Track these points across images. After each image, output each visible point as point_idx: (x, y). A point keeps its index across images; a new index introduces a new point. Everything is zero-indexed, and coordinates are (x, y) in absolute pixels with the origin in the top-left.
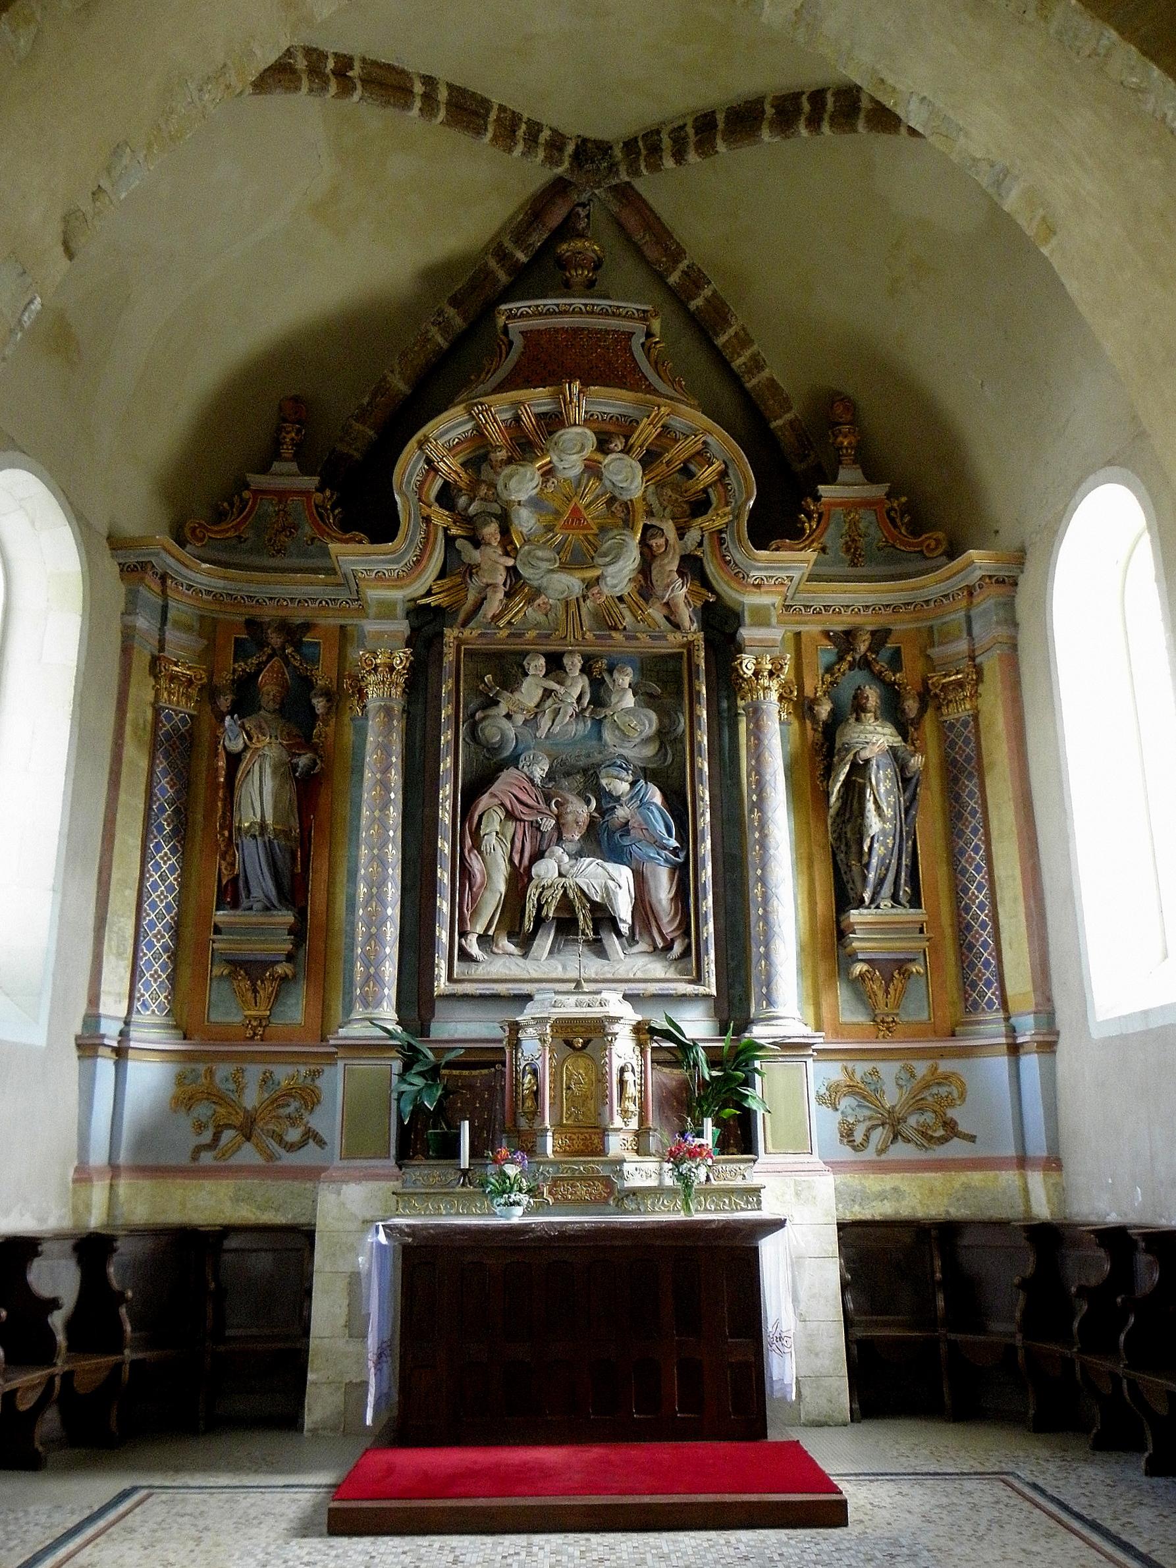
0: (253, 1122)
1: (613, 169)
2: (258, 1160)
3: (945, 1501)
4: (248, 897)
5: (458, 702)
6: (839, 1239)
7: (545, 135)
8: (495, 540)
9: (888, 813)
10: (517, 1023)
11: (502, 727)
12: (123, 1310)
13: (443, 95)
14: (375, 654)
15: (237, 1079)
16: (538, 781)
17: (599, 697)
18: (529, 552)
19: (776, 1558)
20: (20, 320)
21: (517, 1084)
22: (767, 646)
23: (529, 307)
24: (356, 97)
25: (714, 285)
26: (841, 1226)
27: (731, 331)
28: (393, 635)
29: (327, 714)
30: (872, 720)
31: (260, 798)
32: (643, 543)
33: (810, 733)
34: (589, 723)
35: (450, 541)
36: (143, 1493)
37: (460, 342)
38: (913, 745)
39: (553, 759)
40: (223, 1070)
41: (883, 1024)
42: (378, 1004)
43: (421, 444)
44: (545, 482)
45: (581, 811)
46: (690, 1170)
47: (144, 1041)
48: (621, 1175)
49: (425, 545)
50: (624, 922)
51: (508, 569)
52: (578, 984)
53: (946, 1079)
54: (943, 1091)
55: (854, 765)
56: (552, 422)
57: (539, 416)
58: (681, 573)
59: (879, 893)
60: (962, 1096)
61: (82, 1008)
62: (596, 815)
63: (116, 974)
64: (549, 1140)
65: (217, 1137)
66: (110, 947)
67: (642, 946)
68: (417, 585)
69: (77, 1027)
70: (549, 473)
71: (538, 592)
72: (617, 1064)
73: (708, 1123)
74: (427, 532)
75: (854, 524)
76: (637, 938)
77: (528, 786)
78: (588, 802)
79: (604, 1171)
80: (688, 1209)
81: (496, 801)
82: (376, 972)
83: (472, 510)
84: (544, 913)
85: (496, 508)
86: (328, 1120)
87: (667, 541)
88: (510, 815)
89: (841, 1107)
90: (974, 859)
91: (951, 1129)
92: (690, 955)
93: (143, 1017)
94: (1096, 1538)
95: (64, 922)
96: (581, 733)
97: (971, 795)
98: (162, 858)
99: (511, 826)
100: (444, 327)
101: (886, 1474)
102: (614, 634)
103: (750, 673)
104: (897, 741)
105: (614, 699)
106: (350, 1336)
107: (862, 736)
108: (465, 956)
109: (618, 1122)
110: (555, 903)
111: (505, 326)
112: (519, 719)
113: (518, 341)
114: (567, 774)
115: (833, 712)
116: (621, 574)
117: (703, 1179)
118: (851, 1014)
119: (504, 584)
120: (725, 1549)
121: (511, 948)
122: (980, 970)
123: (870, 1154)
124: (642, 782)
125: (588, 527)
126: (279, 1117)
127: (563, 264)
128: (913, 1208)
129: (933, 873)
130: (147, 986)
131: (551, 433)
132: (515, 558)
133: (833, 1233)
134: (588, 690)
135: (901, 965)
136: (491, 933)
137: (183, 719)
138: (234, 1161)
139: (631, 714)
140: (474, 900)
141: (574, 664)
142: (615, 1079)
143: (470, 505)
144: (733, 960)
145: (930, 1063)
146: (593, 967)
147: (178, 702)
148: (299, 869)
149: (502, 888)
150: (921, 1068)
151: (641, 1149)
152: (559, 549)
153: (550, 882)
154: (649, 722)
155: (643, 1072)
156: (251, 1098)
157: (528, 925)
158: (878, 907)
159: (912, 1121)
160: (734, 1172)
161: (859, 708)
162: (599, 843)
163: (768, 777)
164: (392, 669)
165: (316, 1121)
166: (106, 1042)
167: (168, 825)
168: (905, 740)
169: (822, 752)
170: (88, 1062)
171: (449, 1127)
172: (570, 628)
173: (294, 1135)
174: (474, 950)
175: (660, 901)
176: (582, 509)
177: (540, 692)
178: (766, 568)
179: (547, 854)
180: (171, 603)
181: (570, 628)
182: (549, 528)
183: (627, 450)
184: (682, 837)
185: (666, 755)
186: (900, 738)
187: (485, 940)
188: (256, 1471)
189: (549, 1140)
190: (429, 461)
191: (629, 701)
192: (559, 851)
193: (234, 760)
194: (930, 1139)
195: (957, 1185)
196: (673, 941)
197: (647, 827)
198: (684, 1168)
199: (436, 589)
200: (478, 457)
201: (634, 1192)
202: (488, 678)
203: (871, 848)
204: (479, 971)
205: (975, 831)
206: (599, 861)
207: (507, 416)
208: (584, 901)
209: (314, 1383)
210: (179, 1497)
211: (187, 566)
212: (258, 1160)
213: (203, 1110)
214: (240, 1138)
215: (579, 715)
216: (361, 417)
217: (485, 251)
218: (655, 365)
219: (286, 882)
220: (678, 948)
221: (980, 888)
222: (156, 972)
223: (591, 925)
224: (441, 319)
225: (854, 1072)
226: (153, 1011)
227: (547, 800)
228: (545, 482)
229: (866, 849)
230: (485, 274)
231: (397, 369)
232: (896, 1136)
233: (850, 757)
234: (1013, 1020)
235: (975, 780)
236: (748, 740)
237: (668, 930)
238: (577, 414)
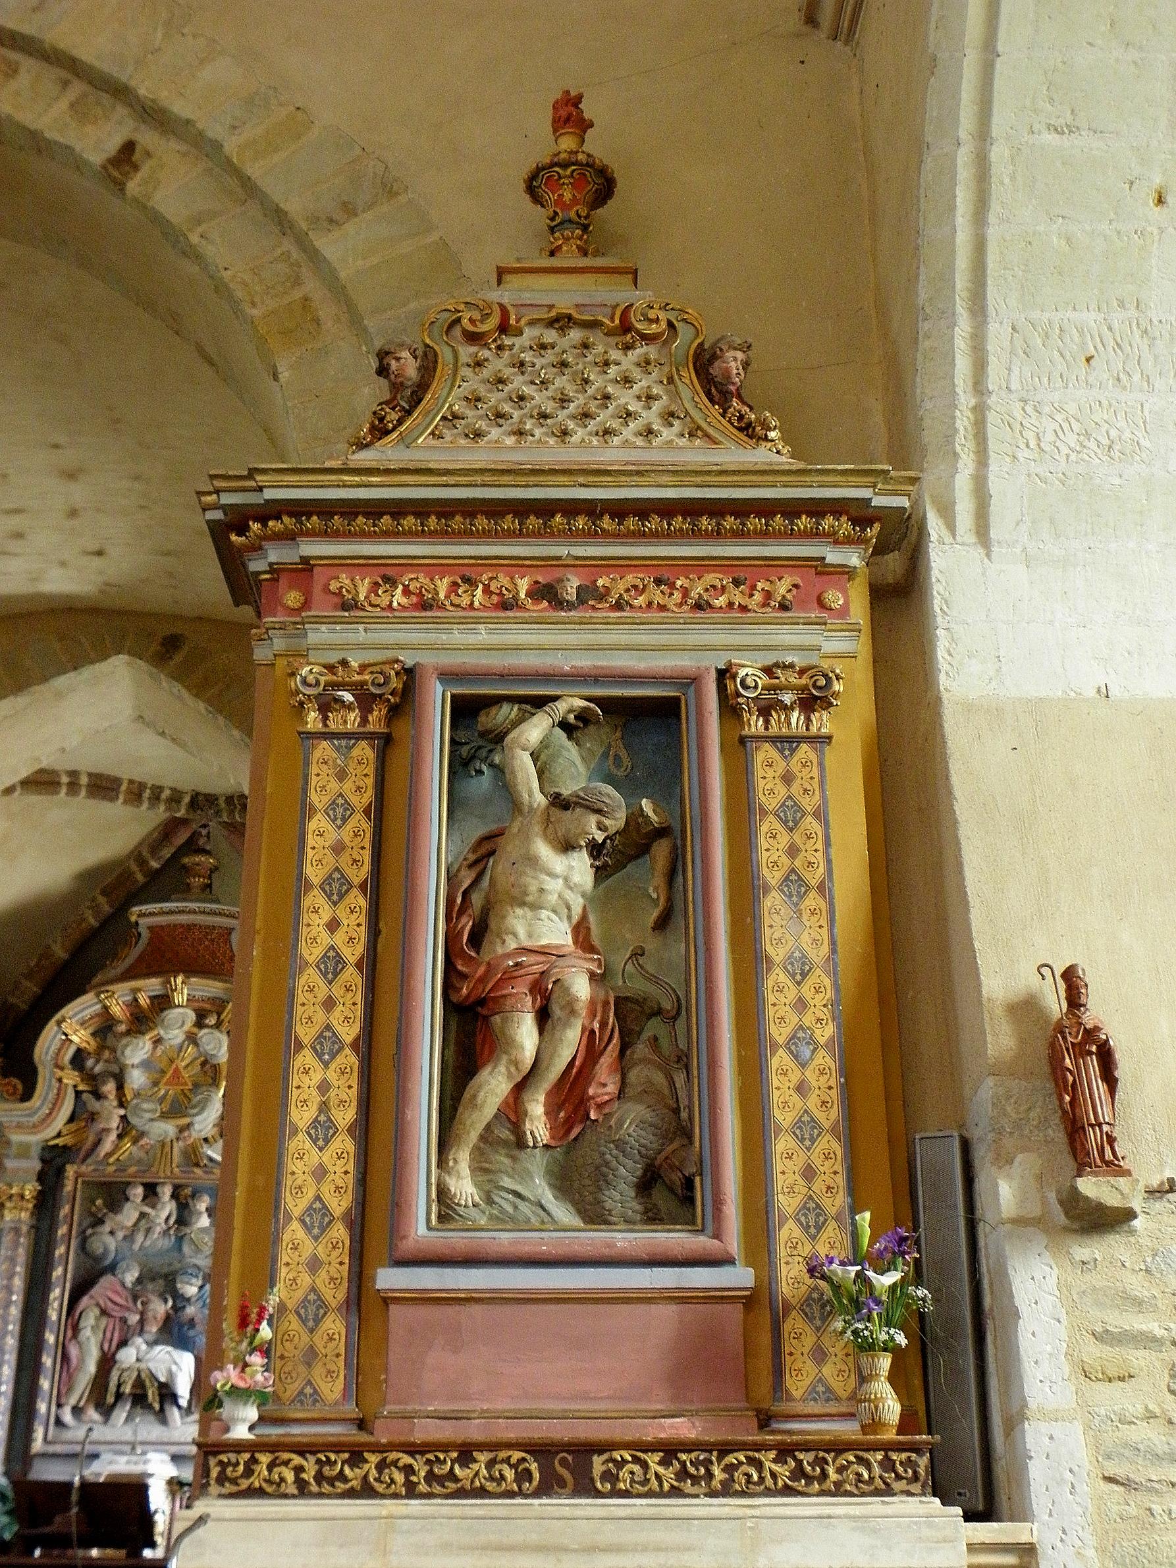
1: (218, 813)
5: (71, 1225)
7: (166, 794)
8: (112, 1096)
11: (107, 1242)
13: (84, 780)
14: (10, 1186)
16: (129, 1285)
17: (183, 1218)
18: (137, 1104)
24: (16, 794)
34: (173, 1239)
35: (78, 1094)
37: (106, 923)
39: (143, 1266)
44: (155, 1048)
45: (160, 1309)
49: (57, 1100)
56: (163, 1002)
57: (152, 998)
68: (50, 1129)
70: (158, 1041)
71: (142, 1134)
74: (59, 1090)
76: (193, 1409)
77: (119, 1288)
78: (166, 1301)
83: (98, 1069)
85: (115, 1069)
88: (104, 1312)
96: (165, 1247)
99: (104, 1321)
100: (95, 908)
102: (196, 1170)
108: (59, 1422)
111: (137, 923)
112: (120, 1235)
113: (145, 934)
114: (153, 1279)
116: (206, 1121)
125: (185, 1084)
127: (186, 870)
131: (162, 1010)
136: (82, 1404)
141: (166, 1192)
152: (161, 1100)
157: (110, 1399)
162: (171, 1333)
164: (22, 1197)
174: (67, 1417)
177: (136, 1215)
182: (156, 1084)
183: (218, 1026)
187: (77, 1411)
192: (139, 1340)
199: (64, 1132)
200: (105, 1028)
202: (99, 1202)
204: (68, 1435)
207: (129, 998)
215: (166, 1232)
216: (29, 976)
217: (129, 856)
227: (135, 1298)
228: (155, 1048)
230: (126, 875)
238: (180, 997)
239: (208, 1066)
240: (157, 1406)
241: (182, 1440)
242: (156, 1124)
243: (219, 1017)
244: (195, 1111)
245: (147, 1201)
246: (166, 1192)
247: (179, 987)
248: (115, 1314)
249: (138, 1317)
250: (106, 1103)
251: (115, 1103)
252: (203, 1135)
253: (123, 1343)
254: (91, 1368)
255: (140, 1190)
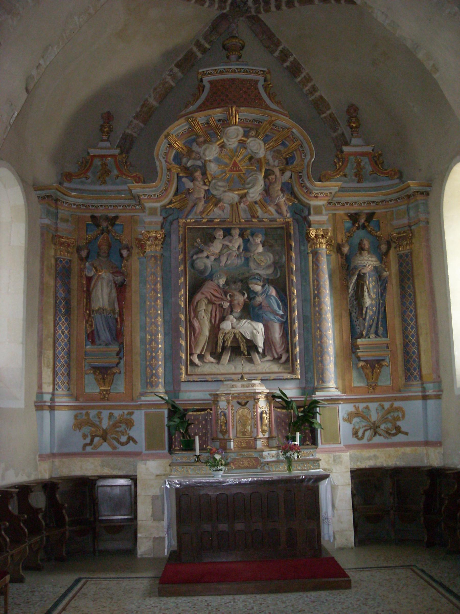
0: (107, 434)
2: (109, 449)
3: (388, 578)
4: (99, 340)
6: (351, 477)
9: (374, 296)
10: (217, 394)
11: (205, 262)
12: (64, 511)
15: (99, 416)
16: (221, 286)
17: (247, 247)
18: (215, 183)
19: (325, 601)
20: (9, 122)
21: (217, 420)
22: (321, 223)
23: (212, 70)
25: (294, 56)
26: (352, 472)
27: (303, 76)
28: (156, 223)
29: (128, 256)
30: (367, 254)
31: (103, 296)
32: (266, 177)
33: (340, 259)
34: (243, 259)
35: (179, 178)
36: (84, 581)
38: (385, 264)
40: (93, 413)
41: (372, 387)
42: (157, 386)
43: (166, 137)
45: (240, 299)
46: (290, 455)
47: (61, 402)
48: (262, 456)
50: (261, 347)
51: (205, 190)
52: (242, 378)
53: (398, 409)
54: (396, 414)
55: (359, 275)
58: (282, 190)
59: (369, 331)
60: (403, 416)
61: (35, 389)
62: (247, 300)
63: (47, 374)
64: (232, 443)
65: (92, 440)
66: (44, 364)
67: (268, 358)
69: (34, 398)
70: (222, 146)
72: (259, 410)
73: (298, 435)
75: (359, 164)
76: (266, 354)
77: (217, 289)
78: (244, 295)
79: (254, 455)
80: (289, 470)
81: (204, 296)
82: (156, 372)
83: (189, 164)
84: (226, 344)
86: (139, 432)
87: (276, 176)
89: (353, 422)
90: (410, 316)
91: (398, 430)
92: (289, 361)
93: (60, 391)
94: (440, 589)
95: (27, 355)
97: (409, 288)
98: (62, 324)
99: (210, 307)
100: (173, 76)
101: (367, 568)
103: (313, 236)
104: (377, 263)
105: (253, 249)
106: (154, 520)
107: (363, 262)
108: (193, 363)
109: (260, 435)
110: (230, 340)
112: (212, 258)
113: (207, 86)
114: (235, 282)
115: (350, 249)
116: (256, 192)
117: (296, 458)
118: (358, 383)
119: (204, 197)
120: (306, 599)
121: (212, 360)
122: (411, 364)
123: (365, 441)
124: (267, 285)
125: (241, 171)
126: (117, 432)
128: (382, 463)
129: (394, 321)
130: (60, 379)
132: (209, 186)
133: (349, 475)
134: (242, 244)
135: (379, 362)
136: (203, 353)
137: (67, 262)
138: (100, 449)
139: (262, 258)
140: (195, 339)
141: (236, 232)
142: (259, 417)
143: (188, 162)
144: (307, 362)
145: (391, 403)
146: (248, 368)
147: (64, 254)
148: (119, 327)
149: (207, 333)
150: (387, 405)
151: (269, 446)
153: (228, 331)
154: (269, 258)
155: (270, 413)
156: (105, 424)
157: (219, 350)
158: (369, 338)
159: (383, 427)
160: (307, 453)
161: (361, 249)
163: (322, 283)
165: (132, 433)
166: (47, 404)
167: (63, 309)
168: (381, 262)
169: (346, 267)
170: (39, 412)
171: (190, 437)
172: (234, 218)
173: (124, 439)
174: (196, 361)
175: (276, 338)
176: (237, 162)
177: (221, 246)
178: (320, 190)
179: (226, 318)
180: (59, 211)
181: (234, 218)
183: (257, 136)
184: (285, 311)
185: (277, 272)
186: (378, 262)
187: (201, 357)
188: (123, 572)
189: (232, 443)
190: (170, 144)
191: (260, 249)
192: (231, 317)
193: (89, 279)
194: (390, 434)
195: (400, 453)
196: (281, 355)
197: (270, 306)
198: (288, 454)
199: (174, 200)
201: (268, 463)
202: (198, 240)
203: (366, 311)
204: (199, 370)
205: (410, 304)
206: (249, 321)
208: (243, 339)
209: (141, 538)
210: (98, 582)
211: (65, 195)
212: (109, 449)
213: (86, 430)
214: (102, 441)
215: (238, 256)
218: (269, 96)
219: (114, 332)
220: (284, 358)
221: (412, 328)
222: (63, 372)
223: (246, 349)
224: (171, 73)
225: (358, 407)
226: (63, 389)
228: (221, 151)
229: (364, 312)
231: (152, 95)
232: (375, 433)
233: (357, 272)
234: (425, 385)
235: (411, 281)
236: (313, 266)
237: (280, 350)
239: (253, 160)
240: (246, 353)
241: (264, 371)
242: (227, 194)
243: (257, 131)
244: (250, 186)
245: (226, 238)
246: (236, 232)
247: (234, 113)
248: (217, 303)
249: (229, 304)
250: (197, 183)
251: (202, 183)
252: (254, 200)
253: (223, 319)
254: (207, 333)
255: (221, 233)
